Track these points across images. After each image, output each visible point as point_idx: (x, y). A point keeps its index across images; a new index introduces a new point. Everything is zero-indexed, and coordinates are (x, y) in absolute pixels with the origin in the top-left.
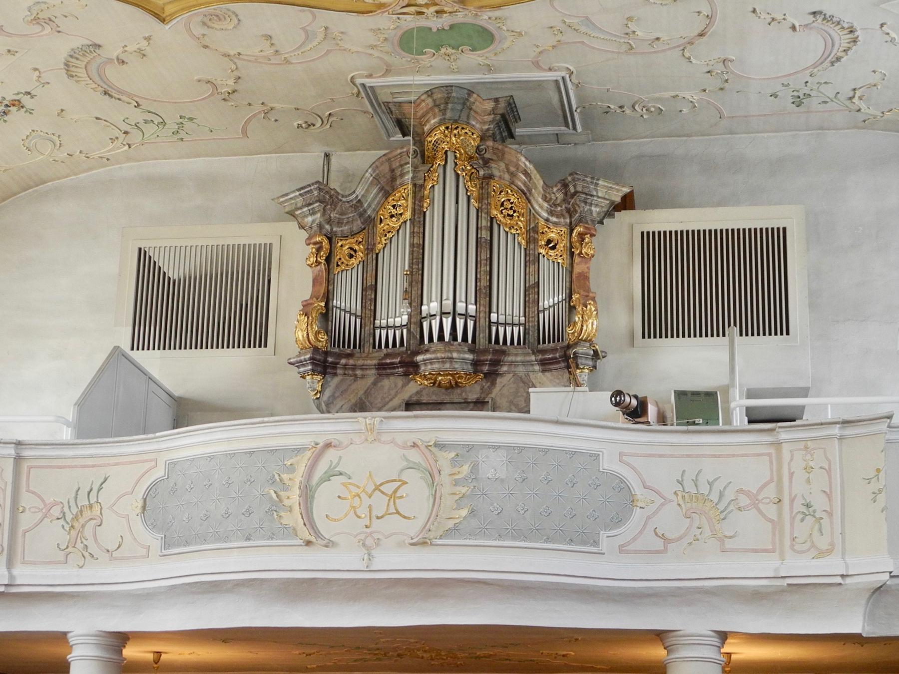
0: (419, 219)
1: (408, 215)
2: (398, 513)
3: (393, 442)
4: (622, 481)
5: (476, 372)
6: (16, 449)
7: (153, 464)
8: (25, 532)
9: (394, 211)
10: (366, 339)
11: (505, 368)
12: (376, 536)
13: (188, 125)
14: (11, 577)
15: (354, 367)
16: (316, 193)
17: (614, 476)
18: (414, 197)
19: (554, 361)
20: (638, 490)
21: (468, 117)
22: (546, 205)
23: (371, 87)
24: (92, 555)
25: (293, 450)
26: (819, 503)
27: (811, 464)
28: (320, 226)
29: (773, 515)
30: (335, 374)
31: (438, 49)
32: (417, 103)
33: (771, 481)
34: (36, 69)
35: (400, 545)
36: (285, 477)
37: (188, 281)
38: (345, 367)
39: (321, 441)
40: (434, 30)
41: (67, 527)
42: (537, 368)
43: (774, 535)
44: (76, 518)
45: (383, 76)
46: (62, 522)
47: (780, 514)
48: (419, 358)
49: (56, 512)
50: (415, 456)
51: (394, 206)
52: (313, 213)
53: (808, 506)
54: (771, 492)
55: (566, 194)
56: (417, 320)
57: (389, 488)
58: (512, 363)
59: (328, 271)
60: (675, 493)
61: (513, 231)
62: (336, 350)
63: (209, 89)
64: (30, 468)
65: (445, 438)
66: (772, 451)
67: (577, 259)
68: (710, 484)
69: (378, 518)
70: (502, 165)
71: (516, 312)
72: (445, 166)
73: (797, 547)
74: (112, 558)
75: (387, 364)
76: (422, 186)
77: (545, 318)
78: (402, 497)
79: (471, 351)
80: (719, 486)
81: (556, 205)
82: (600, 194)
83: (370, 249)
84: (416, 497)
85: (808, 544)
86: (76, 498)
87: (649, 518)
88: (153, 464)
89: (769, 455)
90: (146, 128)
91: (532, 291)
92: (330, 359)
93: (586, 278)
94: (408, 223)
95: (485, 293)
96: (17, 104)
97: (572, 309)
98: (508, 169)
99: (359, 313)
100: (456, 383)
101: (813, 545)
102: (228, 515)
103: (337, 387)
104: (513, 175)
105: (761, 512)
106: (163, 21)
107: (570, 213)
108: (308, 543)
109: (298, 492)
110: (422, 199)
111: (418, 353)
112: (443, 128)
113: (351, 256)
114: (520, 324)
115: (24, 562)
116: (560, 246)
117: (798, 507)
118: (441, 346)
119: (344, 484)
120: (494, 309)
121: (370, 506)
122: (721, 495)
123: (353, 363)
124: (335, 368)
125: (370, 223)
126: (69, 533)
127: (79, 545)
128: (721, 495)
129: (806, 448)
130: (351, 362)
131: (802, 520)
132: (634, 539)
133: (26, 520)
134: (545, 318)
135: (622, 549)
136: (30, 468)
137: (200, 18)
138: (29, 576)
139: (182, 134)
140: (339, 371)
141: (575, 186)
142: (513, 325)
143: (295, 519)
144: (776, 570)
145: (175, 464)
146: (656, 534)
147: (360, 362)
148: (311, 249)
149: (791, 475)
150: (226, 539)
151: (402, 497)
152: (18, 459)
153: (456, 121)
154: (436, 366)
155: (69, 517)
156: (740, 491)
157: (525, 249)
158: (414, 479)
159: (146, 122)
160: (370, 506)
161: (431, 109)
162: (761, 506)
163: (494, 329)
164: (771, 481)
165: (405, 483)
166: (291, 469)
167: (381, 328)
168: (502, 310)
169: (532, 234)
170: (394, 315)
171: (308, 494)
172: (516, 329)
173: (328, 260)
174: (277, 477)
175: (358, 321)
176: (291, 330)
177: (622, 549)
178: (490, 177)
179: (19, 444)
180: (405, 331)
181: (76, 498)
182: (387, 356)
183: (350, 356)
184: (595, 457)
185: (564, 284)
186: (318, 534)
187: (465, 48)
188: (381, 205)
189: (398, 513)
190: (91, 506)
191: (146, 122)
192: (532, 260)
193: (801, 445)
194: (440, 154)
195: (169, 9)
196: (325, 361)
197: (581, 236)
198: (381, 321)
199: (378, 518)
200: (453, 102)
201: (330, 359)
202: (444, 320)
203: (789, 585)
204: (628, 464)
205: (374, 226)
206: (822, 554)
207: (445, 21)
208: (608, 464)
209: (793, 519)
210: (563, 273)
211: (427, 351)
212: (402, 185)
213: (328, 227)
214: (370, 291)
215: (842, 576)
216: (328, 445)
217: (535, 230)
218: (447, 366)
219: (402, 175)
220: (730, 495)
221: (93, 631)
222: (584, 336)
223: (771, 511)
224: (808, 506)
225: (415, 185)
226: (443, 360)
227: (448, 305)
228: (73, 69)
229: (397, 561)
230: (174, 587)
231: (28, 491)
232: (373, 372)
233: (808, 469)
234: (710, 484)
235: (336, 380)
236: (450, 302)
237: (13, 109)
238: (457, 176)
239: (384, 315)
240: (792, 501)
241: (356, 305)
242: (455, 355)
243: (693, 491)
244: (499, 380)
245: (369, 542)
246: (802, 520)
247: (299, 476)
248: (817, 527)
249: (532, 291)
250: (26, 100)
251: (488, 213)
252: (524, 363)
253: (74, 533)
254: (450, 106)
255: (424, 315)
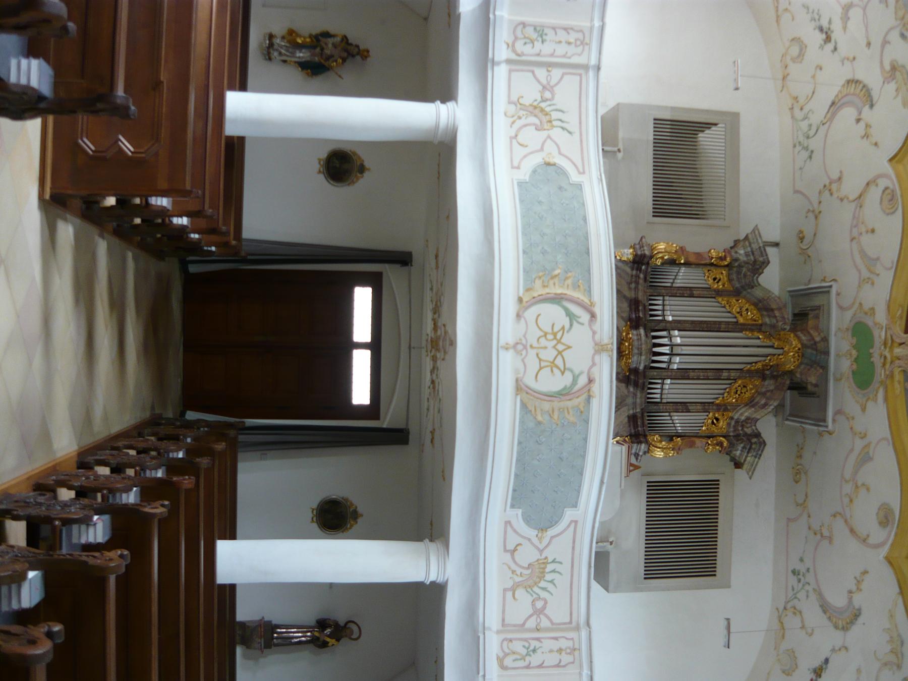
0: (735, 327)
1: (741, 320)
2: (541, 368)
3: (594, 364)
4: (556, 522)
5: (630, 370)
6: (594, 66)
7: (581, 170)
8: (533, 72)
9: (744, 309)
10: (656, 290)
11: (631, 389)
12: (524, 353)
13: (805, 154)
14: (499, 63)
15: (637, 283)
16: (761, 259)
17: (560, 517)
18: (753, 325)
19: (636, 426)
20: (551, 532)
21: (806, 364)
22: (743, 418)
23: (828, 292)
24: (513, 123)
25: (590, 287)
26: (535, 660)
27: (563, 653)
28: (736, 260)
29: (528, 625)
30: (632, 269)
31: (854, 347)
32: (816, 328)
33: (552, 623)
34: (854, 58)
35: (517, 371)
36: (569, 281)
37: (694, 144)
38: (638, 276)
39: (597, 310)
40: (871, 351)
41: (535, 104)
42: (631, 412)
43: (515, 626)
44: (542, 110)
45: (837, 304)
46: (539, 99)
47: (530, 630)
48: (642, 331)
49: (548, 95)
50: (582, 381)
51: (747, 310)
52: (747, 255)
53: (534, 651)
54: (545, 623)
55: (750, 435)
56: (668, 327)
57: (559, 361)
58: (635, 395)
59: (705, 265)
60: (546, 558)
61: (726, 395)
62: (649, 270)
63: (835, 176)
64: (580, 75)
65: (595, 402)
66: (574, 624)
67: (704, 440)
68: (552, 582)
69: (537, 355)
70: (772, 388)
71: (669, 396)
72: (772, 347)
73: (505, 643)
74: (511, 138)
75: (638, 307)
76: (760, 331)
77: (665, 418)
78: (552, 371)
79: (645, 367)
80: (550, 587)
81: (742, 426)
82: (749, 458)
83: (718, 293)
84: (552, 382)
85: (507, 651)
86: (557, 110)
87: (529, 540)
88: (581, 170)
89: (571, 622)
90: (806, 122)
91: (683, 407)
92: (643, 267)
93: (691, 447)
94: (735, 320)
95: (684, 374)
96: (828, 39)
97: (671, 438)
98: (768, 391)
99: (674, 285)
100: (623, 356)
101: (506, 655)
102: (543, 235)
103: (624, 271)
104: (764, 394)
105: (531, 616)
106: (891, 160)
107: (737, 436)
108: (520, 300)
109: (559, 291)
110: (752, 330)
111: (645, 329)
112: (799, 346)
113: (715, 279)
114: (661, 399)
115: (510, 71)
116: (714, 428)
117: (534, 644)
118: (649, 346)
119: (563, 328)
120: (673, 381)
121: (546, 348)
122: (544, 589)
123: (641, 278)
124: (637, 270)
125: (737, 293)
126: (531, 105)
127: (522, 113)
128: (544, 589)
129: (575, 650)
130: (641, 281)
131: (524, 646)
132: (515, 531)
133: (541, 73)
134: (665, 418)
135: (508, 523)
136: (580, 75)
137: (891, 187)
138: (500, 75)
139: (798, 148)
140: (634, 272)
141: (755, 443)
142: (661, 394)
143: (539, 291)
144: (490, 629)
145: (581, 189)
146: (518, 545)
147: (640, 287)
148: (722, 254)
149: (556, 639)
150: (524, 234)
151: (552, 371)
152: (586, 67)
153: (803, 355)
154: (636, 343)
155: (543, 105)
156: (546, 602)
157: (712, 403)
158: (568, 379)
159: (810, 125)
160: (546, 348)
161: (813, 339)
162: (535, 617)
163: (660, 381)
164: (552, 623)
165: (563, 373)
166: (576, 287)
167: (664, 300)
168: (671, 391)
169: (723, 408)
170: (671, 310)
171: (557, 299)
172: (658, 396)
173: (712, 264)
174: (570, 274)
175: (669, 285)
176: (665, 240)
177: (508, 523)
178: (764, 378)
179: (598, 68)
180: (660, 318)
181: (557, 110)
182: (644, 306)
183: (645, 280)
184: (575, 505)
185: (688, 431)
186: (527, 308)
187: (855, 367)
188: (748, 301)
189: (541, 368)
190: (550, 122)
191: (810, 125)
192: (705, 407)
193: (577, 646)
194: (781, 343)
195: (900, 167)
196: (643, 264)
197: (720, 444)
198: (669, 301)
199: (537, 355)
200: (816, 355)
201: (643, 267)
202: (668, 348)
203: (479, 637)
204: (569, 526)
205: (735, 296)
206: (500, 661)
207: (877, 360)
208: (569, 514)
209: (526, 640)
210: (695, 430)
211: (646, 336)
212: (762, 315)
213: (736, 264)
214: (688, 292)
215: (484, 676)
216: (593, 316)
217: (726, 410)
218: (636, 351)
219: (769, 316)
220: (543, 594)
221: (457, 122)
222: (652, 448)
223: (531, 623)
224: (534, 651)
225: (761, 325)
226: (639, 349)
227: (677, 350)
228: (853, 85)
229: (506, 370)
230: (489, 190)
231: (563, 74)
232: (633, 296)
233: (560, 651)
234: (552, 582)
235: (628, 270)
236: (680, 352)
237: (824, 36)
238: (767, 356)
239: (672, 303)
240: (538, 639)
241: (679, 283)
242: (643, 357)
243: (547, 570)
244: (623, 385)
245: (520, 347)
246: (524, 646)
247: (570, 293)
248: (519, 657)
249: (683, 407)
250: (830, 46)
251: (739, 378)
252: (635, 403)
253: (531, 109)
254: (815, 352)
255: (672, 332)
